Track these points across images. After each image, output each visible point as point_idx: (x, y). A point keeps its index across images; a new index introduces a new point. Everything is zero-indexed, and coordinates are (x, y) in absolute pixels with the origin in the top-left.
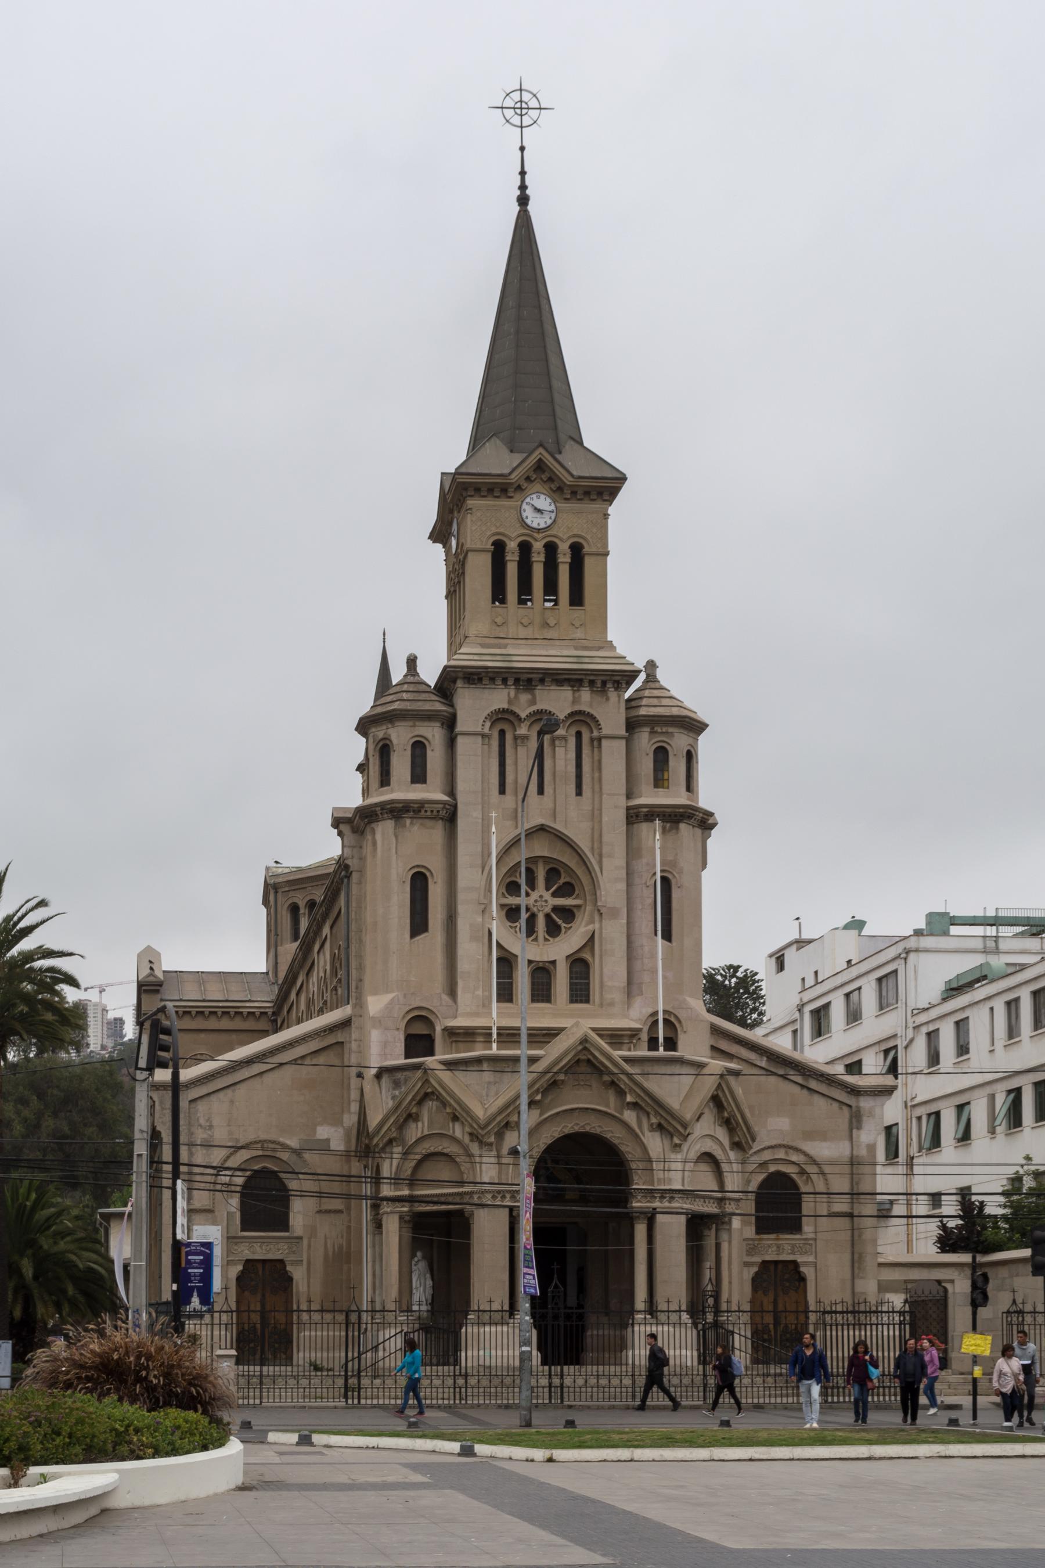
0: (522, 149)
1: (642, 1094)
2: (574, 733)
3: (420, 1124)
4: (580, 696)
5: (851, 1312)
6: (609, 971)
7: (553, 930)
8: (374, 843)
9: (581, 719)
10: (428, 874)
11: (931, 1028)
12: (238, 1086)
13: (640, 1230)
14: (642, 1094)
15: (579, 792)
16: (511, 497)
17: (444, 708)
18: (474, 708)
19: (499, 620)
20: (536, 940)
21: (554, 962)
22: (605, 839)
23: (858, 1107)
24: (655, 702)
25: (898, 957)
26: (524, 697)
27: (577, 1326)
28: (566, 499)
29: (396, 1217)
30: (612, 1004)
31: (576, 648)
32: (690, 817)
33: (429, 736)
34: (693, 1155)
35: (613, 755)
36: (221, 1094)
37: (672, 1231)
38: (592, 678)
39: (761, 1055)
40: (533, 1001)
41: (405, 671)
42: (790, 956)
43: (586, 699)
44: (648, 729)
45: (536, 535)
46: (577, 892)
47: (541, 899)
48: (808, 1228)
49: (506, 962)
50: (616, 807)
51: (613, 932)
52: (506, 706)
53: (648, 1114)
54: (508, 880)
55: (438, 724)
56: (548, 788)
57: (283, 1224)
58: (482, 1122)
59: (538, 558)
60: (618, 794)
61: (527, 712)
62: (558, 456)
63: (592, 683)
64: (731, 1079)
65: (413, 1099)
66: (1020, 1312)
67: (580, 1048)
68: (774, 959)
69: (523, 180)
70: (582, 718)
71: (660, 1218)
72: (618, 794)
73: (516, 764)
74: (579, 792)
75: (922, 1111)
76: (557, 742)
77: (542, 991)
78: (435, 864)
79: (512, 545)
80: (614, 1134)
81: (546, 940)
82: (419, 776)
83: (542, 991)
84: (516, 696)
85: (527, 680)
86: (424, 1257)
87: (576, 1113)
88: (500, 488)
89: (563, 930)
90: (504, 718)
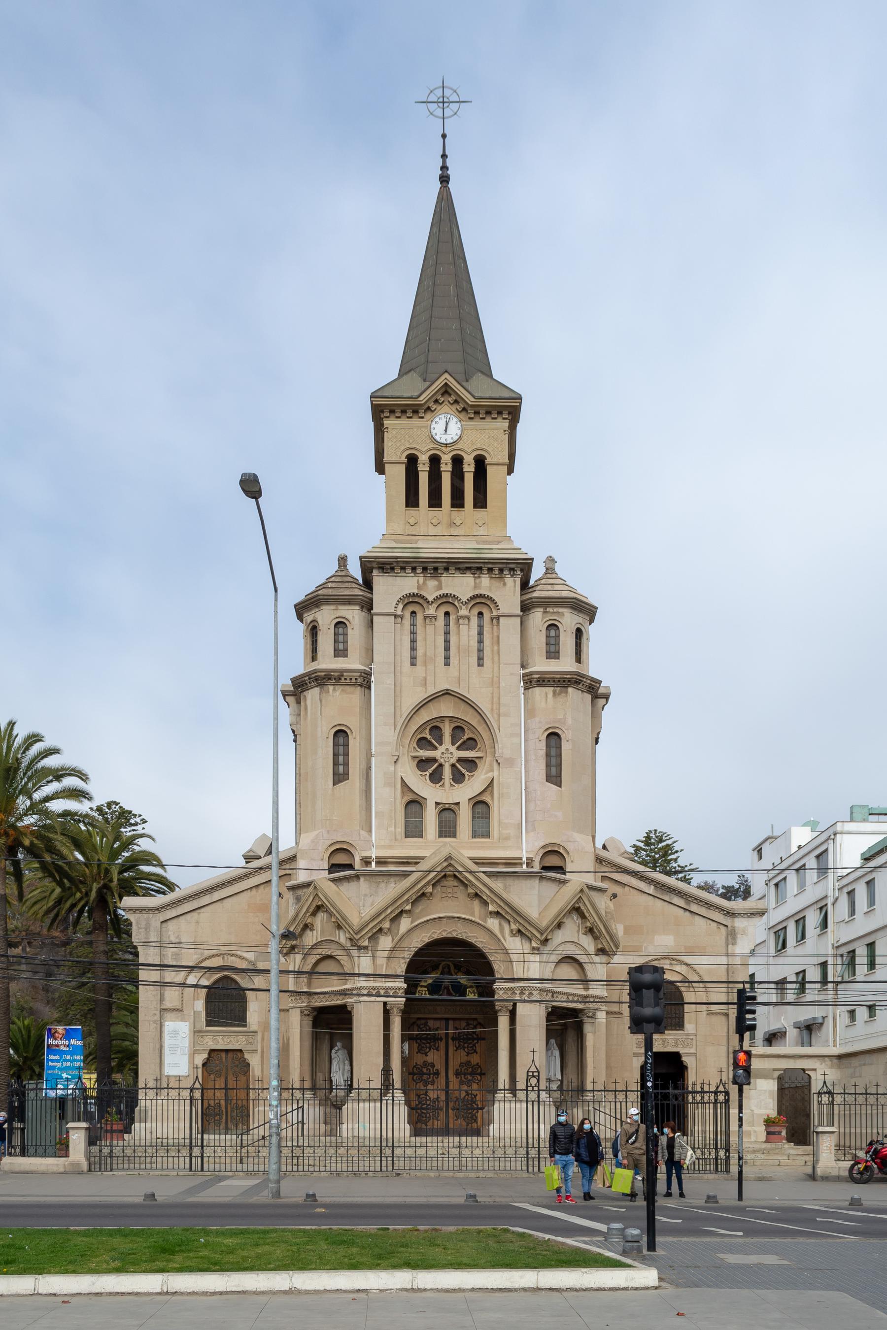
0: (444, 136)
1: (502, 904)
2: (476, 614)
3: (315, 932)
4: (481, 582)
5: (706, 1092)
6: (502, 812)
7: (458, 777)
8: (306, 709)
9: (480, 601)
10: (348, 731)
11: (850, 888)
12: (203, 910)
13: (503, 1022)
14: (502, 904)
15: (480, 664)
16: (422, 418)
17: (361, 593)
18: (388, 591)
19: (412, 521)
20: (443, 785)
21: (458, 804)
22: (502, 701)
23: (733, 927)
24: (549, 587)
25: (829, 838)
26: (432, 583)
27: (662, 1105)
28: (470, 418)
29: (298, 1011)
30: (507, 838)
31: (478, 543)
32: (577, 682)
33: (349, 617)
34: (555, 958)
35: (510, 630)
36: (188, 916)
37: (532, 1020)
38: (490, 566)
39: (650, 884)
40: (440, 836)
41: (336, 567)
42: (766, 848)
43: (485, 585)
44: (542, 610)
45: (444, 449)
46: (479, 746)
47: (447, 752)
48: (689, 1027)
49: (414, 804)
50: (512, 674)
51: (505, 778)
52: (416, 591)
53: (509, 922)
54: (419, 736)
55: (357, 607)
56: (453, 660)
57: (240, 1018)
58: (356, 928)
59: (446, 468)
60: (514, 664)
61: (434, 596)
62: (464, 384)
63: (490, 570)
64: (593, 894)
65: (307, 911)
66: (830, 1093)
67: (445, 864)
68: (756, 852)
69: (444, 162)
70: (483, 600)
71: (520, 1007)
72: (514, 664)
73: (425, 639)
74: (480, 664)
75: (844, 950)
76: (461, 621)
77: (447, 829)
78: (353, 723)
79: (423, 460)
80: (478, 939)
81: (451, 785)
82: (340, 652)
83: (447, 829)
84: (424, 583)
85: (434, 568)
86: (344, 1047)
87: (444, 921)
88: (414, 410)
89: (467, 777)
90: (413, 601)
